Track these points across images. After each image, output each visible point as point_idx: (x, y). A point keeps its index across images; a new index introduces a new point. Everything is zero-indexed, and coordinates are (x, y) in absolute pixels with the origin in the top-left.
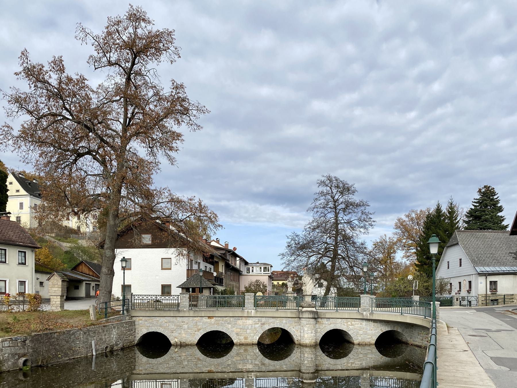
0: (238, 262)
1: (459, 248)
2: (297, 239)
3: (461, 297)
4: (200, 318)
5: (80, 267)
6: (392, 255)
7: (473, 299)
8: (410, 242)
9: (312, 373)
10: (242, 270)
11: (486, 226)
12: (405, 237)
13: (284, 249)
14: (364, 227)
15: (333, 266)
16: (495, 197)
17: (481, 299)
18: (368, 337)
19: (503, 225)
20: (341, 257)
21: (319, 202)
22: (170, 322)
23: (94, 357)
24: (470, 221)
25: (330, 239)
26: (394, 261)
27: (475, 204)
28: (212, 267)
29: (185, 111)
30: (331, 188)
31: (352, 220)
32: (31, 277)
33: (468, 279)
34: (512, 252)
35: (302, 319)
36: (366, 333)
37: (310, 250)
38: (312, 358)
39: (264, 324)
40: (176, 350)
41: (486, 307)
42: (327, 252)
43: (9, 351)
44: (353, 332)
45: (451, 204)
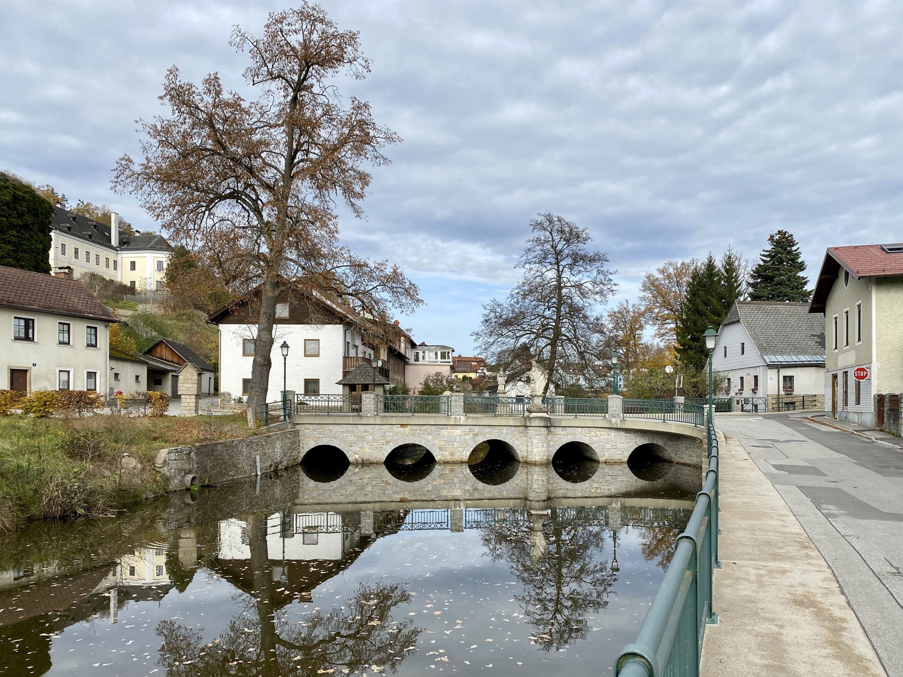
0: (403, 345)
1: (741, 328)
2: (499, 310)
3: (743, 399)
4: (390, 426)
5: (159, 350)
6: (637, 333)
7: (760, 401)
8: (666, 312)
9: (544, 501)
10: (407, 356)
11: (780, 292)
12: (657, 304)
13: (479, 327)
14: (601, 293)
15: (553, 352)
16: (794, 248)
17: (771, 401)
18: (619, 452)
19: (806, 290)
20: (565, 338)
21: (534, 254)
22: (348, 432)
23: (259, 477)
24: (757, 283)
25: (549, 310)
26: (640, 342)
27: (765, 258)
28: (372, 352)
29: (367, 139)
30: (551, 233)
31: (582, 282)
33: (753, 373)
34: (814, 334)
35: (530, 428)
36: (615, 447)
37: (519, 328)
38: (543, 481)
39: (477, 435)
40: (357, 470)
41: (778, 413)
42: (545, 330)
43: (175, 466)
44: (597, 445)
45: (730, 257)
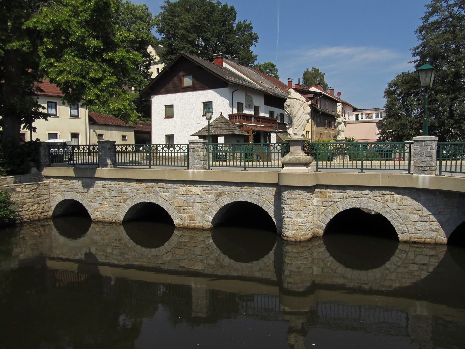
32: (85, 129)
